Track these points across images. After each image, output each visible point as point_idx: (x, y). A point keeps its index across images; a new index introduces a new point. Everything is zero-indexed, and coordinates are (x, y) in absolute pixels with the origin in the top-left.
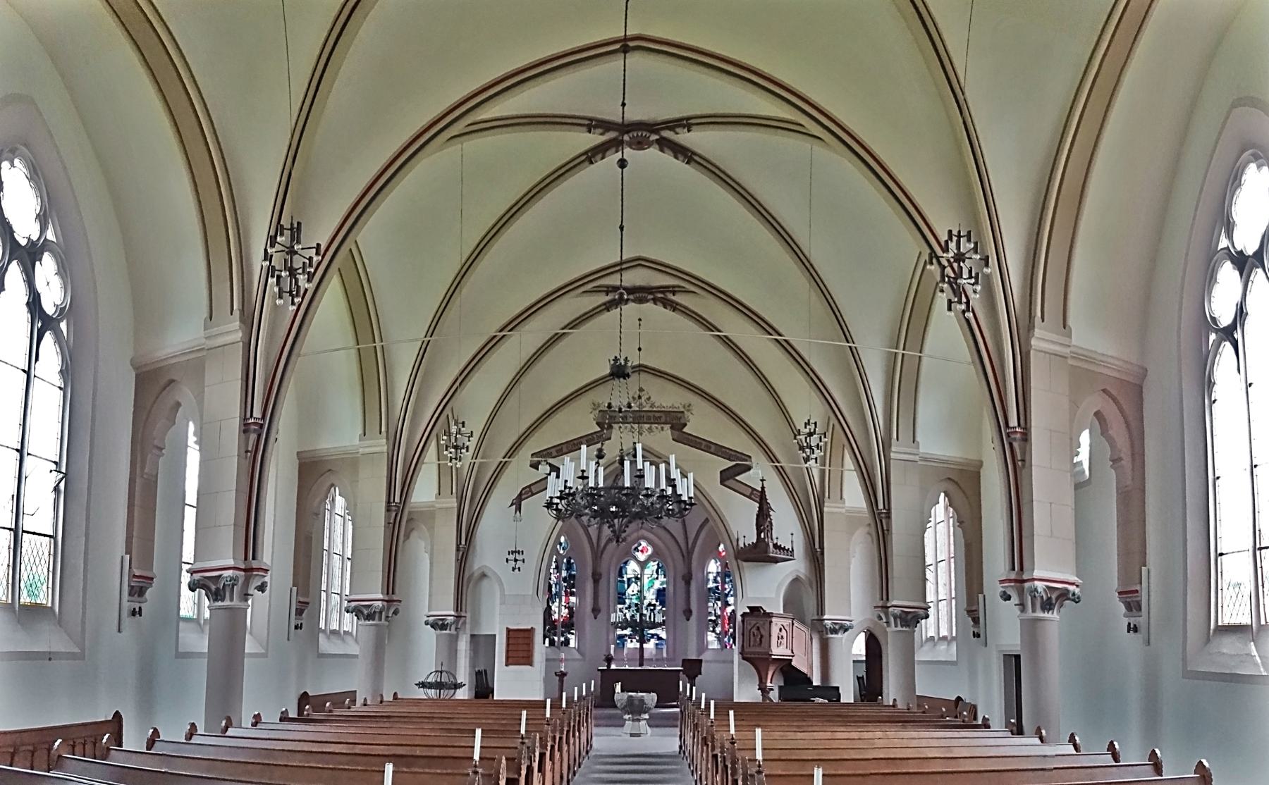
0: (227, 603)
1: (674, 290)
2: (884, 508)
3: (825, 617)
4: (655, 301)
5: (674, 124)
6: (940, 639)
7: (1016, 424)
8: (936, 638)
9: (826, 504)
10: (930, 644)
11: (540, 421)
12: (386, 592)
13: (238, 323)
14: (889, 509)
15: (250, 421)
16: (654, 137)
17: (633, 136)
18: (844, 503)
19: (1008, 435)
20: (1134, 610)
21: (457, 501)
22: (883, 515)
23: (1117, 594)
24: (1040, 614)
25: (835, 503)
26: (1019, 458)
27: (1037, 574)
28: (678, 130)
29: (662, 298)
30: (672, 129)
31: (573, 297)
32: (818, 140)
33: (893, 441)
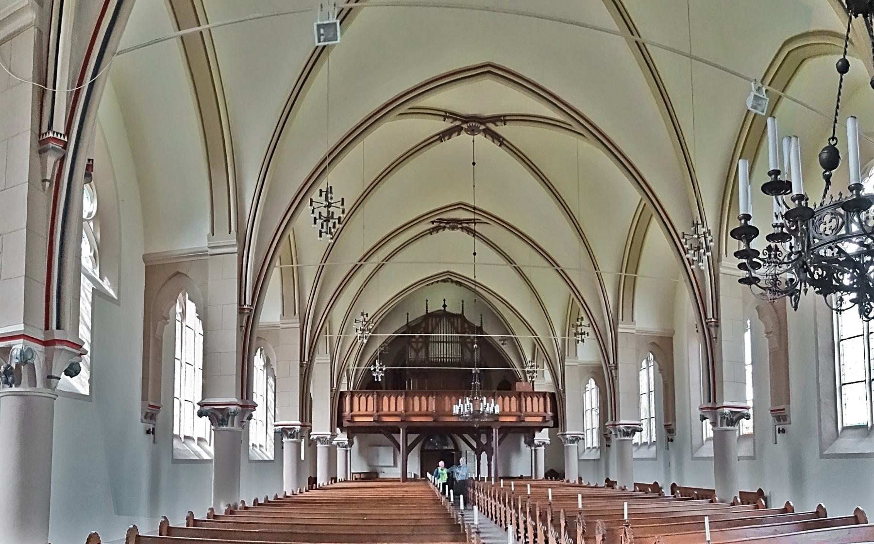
0: (229, 427)
1: (475, 222)
2: (614, 363)
3: (567, 433)
4: (462, 228)
5: (496, 119)
6: (594, 448)
7: (712, 317)
8: (639, 444)
9: (566, 360)
10: (588, 450)
11: (518, 315)
12: (301, 420)
13: (235, 240)
14: (617, 364)
15: (245, 307)
16: (482, 127)
17: (470, 125)
18: (578, 359)
19: (707, 323)
20: (782, 421)
21: (330, 359)
22: (613, 368)
23: (770, 411)
24: (725, 427)
25: (322, 356)
26: (714, 336)
27: (725, 404)
28: (498, 123)
29: (466, 227)
30: (494, 123)
31: (425, 224)
32: (580, 136)
33: (620, 321)
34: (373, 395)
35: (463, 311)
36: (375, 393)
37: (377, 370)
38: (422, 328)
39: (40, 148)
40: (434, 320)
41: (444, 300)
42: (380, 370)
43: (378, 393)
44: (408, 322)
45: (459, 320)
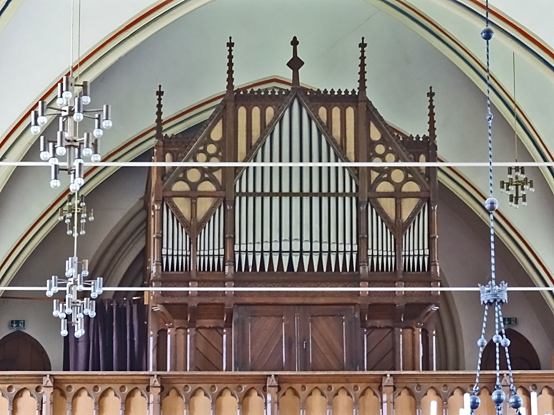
34: (38, 389)
35: (362, 81)
36: (48, 381)
37: (71, 297)
38: (213, 142)
39: (189, 306)
40: (256, 111)
41: (295, 42)
42: (82, 295)
43: (57, 384)
44: (159, 120)
45: (350, 112)
